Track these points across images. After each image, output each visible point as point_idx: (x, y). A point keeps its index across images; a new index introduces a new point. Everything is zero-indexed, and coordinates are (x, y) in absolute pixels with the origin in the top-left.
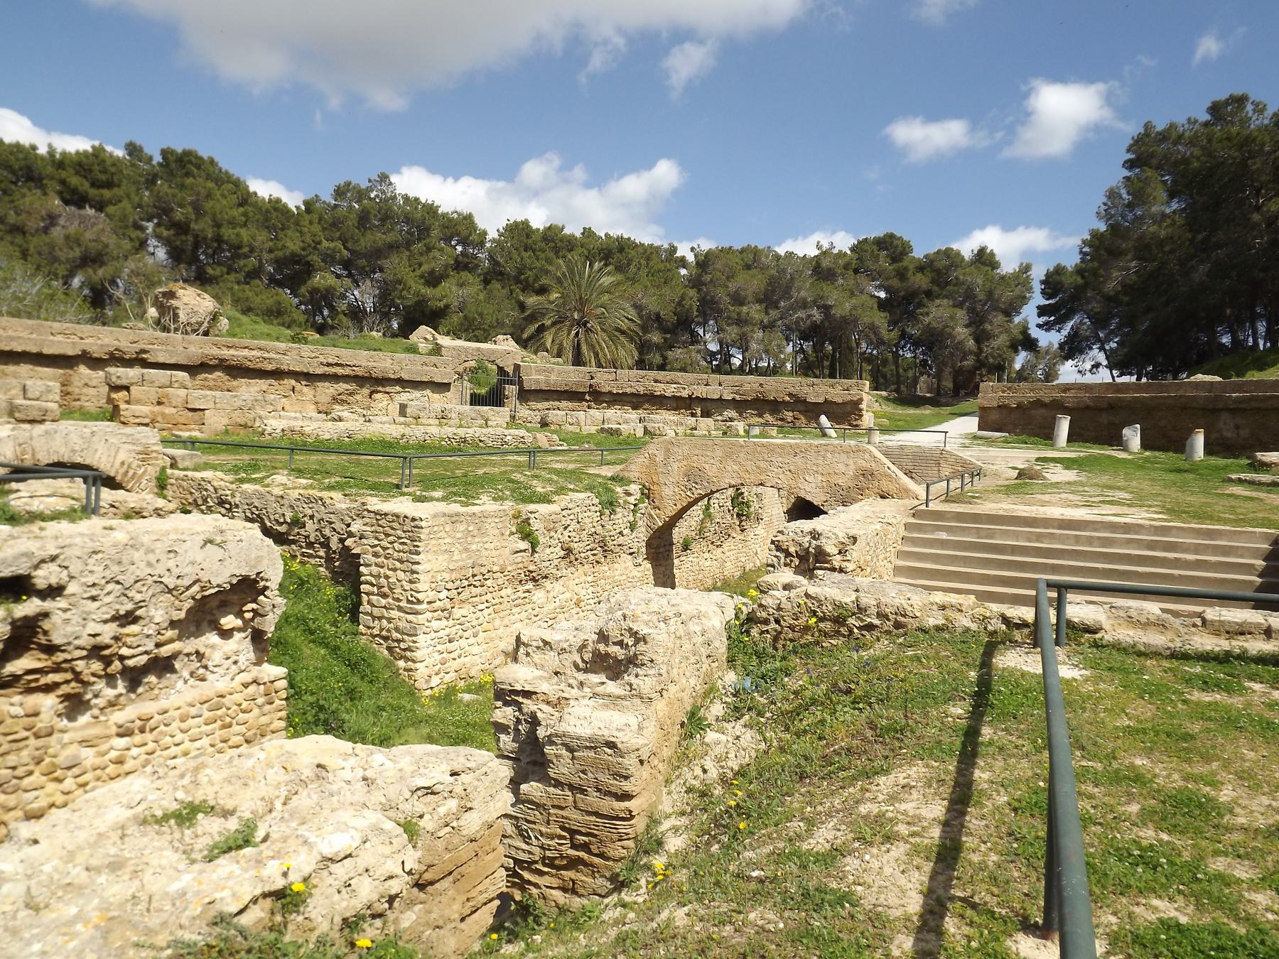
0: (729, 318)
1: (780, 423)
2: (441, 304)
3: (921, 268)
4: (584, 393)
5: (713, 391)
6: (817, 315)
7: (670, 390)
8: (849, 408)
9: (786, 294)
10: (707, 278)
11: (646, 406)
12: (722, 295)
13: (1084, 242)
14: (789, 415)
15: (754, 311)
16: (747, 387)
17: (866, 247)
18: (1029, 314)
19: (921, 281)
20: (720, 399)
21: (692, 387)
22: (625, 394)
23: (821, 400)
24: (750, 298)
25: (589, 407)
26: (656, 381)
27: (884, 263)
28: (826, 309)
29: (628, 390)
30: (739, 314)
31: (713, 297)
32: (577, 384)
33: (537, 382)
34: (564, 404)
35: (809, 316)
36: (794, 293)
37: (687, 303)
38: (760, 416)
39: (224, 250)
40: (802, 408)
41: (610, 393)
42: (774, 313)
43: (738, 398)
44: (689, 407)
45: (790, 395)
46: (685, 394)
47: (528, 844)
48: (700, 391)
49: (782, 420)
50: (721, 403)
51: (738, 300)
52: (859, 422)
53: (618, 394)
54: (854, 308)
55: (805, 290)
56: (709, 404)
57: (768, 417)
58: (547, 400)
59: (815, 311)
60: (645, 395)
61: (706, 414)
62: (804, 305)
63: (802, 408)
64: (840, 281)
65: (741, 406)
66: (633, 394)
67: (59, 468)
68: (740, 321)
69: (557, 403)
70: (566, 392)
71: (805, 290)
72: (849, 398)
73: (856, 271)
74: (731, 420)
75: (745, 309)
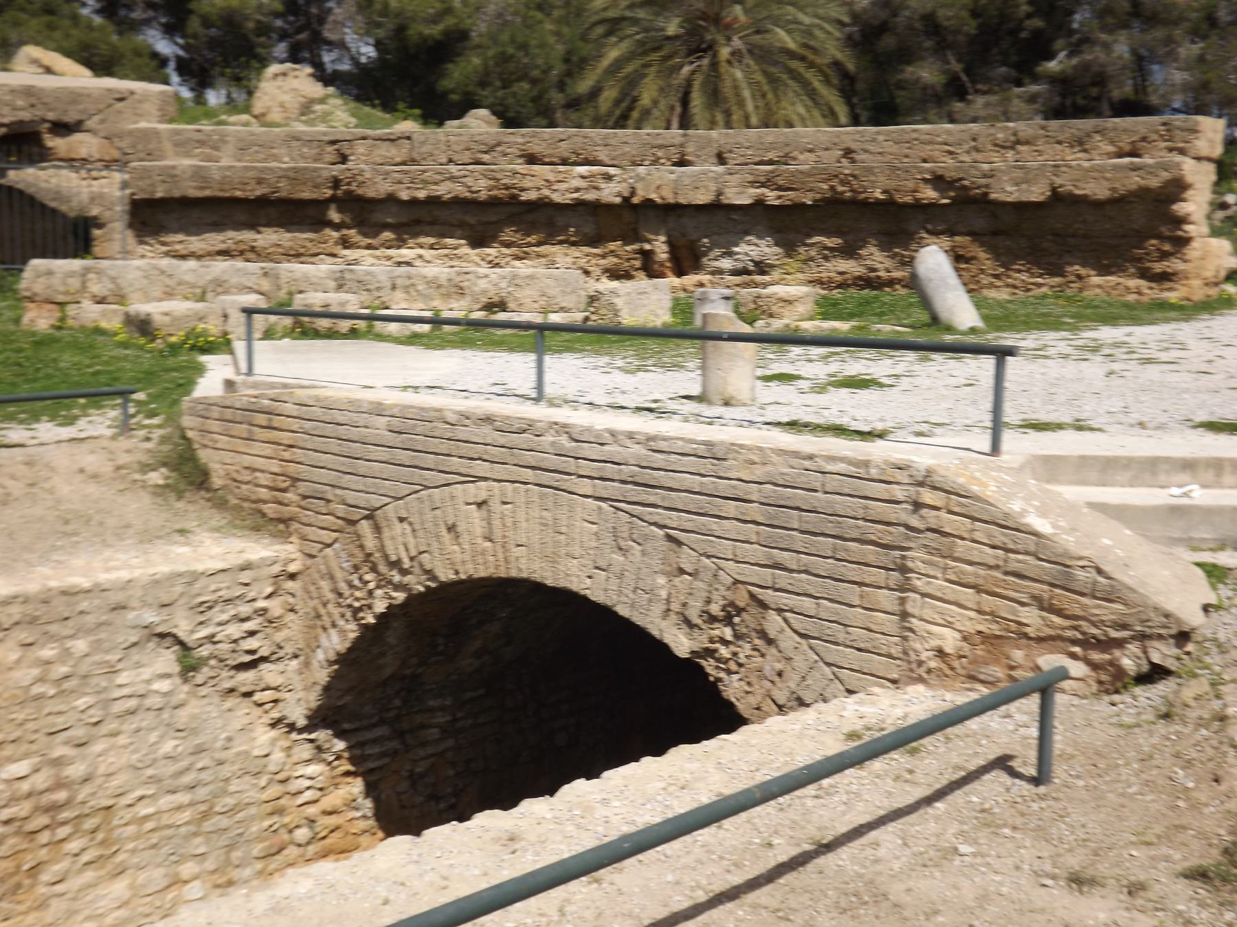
2: (435, 31)
4: (323, 204)
5: (698, 183)
7: (568, 184)
11: (508, 234)
16: (805, 162)
20: (716, 207)
22: (433, 201)
23: (1037, 193)
25: (346, 243)
26: (532, 159)
29: (445, 190)
32: (295, 176)
33: (170, 175)
34: (268, 237)
38: (849, 251)
39: (1185, 87)
40: (980, 223)
41: (391, 199)
43: (772, 197)
44: (632, 235)
45: (938, 181)
46: (610, 193)
47: (357, 809)
48: (660, 182)
52: (1175, 265)
53: (414, 202)
57: (876, 259)
58: (218, 227)
60: (493, 203)
61: (685, 259)
65: (788, 223)
66: (457, 202)
67: (324, 838)
69: (247, 235)
70: (262, 201)
72: (1135, 181)
74: (762, 267)
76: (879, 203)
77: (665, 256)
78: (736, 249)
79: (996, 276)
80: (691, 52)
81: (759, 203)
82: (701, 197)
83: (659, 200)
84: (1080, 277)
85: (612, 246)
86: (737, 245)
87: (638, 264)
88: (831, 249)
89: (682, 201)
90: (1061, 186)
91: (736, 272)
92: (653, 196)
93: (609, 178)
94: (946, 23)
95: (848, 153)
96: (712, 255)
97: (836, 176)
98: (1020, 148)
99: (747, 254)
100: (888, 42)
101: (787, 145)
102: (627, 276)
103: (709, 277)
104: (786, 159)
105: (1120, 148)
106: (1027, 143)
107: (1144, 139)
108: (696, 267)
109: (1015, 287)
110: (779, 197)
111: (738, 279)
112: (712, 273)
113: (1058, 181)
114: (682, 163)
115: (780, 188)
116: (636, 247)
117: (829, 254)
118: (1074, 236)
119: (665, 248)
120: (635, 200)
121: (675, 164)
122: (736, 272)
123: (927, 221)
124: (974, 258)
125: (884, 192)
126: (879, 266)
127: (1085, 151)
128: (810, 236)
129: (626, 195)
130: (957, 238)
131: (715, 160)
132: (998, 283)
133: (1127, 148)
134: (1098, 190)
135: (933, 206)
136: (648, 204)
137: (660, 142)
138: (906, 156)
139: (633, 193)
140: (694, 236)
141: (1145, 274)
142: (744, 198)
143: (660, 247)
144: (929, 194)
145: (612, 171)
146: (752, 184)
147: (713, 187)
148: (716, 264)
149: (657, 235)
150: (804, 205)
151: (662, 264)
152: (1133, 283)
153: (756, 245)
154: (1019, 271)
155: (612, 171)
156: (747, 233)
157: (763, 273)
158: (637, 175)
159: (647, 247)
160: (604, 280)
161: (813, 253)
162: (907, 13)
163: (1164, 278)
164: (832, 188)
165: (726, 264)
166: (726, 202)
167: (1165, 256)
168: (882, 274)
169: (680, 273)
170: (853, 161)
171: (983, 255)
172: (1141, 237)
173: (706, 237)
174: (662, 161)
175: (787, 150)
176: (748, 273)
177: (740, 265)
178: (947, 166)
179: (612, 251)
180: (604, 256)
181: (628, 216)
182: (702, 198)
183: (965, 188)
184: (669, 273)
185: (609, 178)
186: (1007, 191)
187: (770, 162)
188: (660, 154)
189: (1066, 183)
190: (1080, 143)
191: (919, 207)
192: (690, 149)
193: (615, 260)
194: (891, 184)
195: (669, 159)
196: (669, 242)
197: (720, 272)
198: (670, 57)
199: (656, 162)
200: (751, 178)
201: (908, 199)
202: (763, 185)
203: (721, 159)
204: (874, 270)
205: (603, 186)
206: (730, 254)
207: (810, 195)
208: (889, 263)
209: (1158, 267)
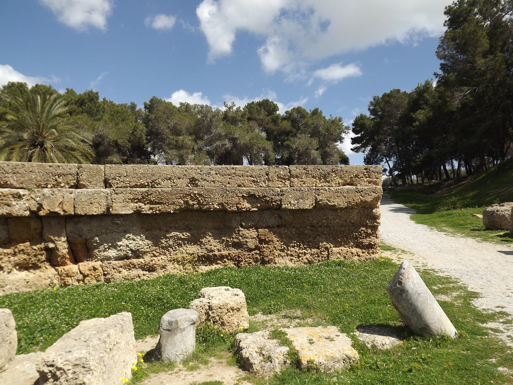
0: (170, 144)
1: (234, 252)
3: (284, 119)
5: (92, 199)
6: (228, 145)
8: (354, 216)
9: (208, 131)
10: (153, 116)
12: (163, 127)
13: (371, 103)
14: (250, 235)
15: (188, 140)
16: (166, 187)
17: (252, 106)
18: (346, 146)
19: (287, 125)
21: (38, 193)
23: (308, 204)
24: (184, 131)
27: (263, 115)
28: (233, 140)
30: (177, 141)
31: (157, 129)
35: (223, 145)
36: (214, 131)
37: (138, 133)
38: (195, 240)
40: (272, 221)
42: (200, 143)
43: (146, 209)
44: (38, 237)
45: (251, 197)
48: (60, 200)
49: (237, 245)
50: (111, 224)
51: (176, 132)
52: (373, 240)
54: (252, 139)
55: (220, 129)
56: (84, 228)
57: (213, 244)
59: (227, 142)
61: (80, 252)
62: (219, 137)
63: (272, 221)
64: (240, 124)
68: (179, 147)
71: (220, 129)
72: (358, 198)
73: (249, 119)
75: (181, 138)
76: (215, 210)
77: (65, 251)
78: (119, 243)
79: (282, 250)
80: (31, 146)
81: (138, 213)
82: (95, 210)
83: (62, 213)
84: (327, 249)
85: (21, 246)
86: (120, 240)
87: (43, 258)
88: (183, 240)
89: (79, 212)
90: (321, 200)
91: (119, 258)
92: (57, 210)
93: (19, 197)
94: (120, 144)
95: (193, 181)
96: (101, 248)
97: (190, 195)
98: (292, 179)
99: (127, 246)
100: (101, 148)
101: (153, 175)
102: (35, 267)
103: (100, 263)
104: (153, 184)
105: (346, 181)
106: (297, 177)
107: (356, 176)
108: (89, 255)
109: (292, 255)
110: (151, 209)
111: (121, 263)
112: (102, 260)
113: (319, 198)
114: (77, 186)
115: (151, 203)
116: (43, 245)
117: (180, 242)
118: (321, 226)
119: (66, 245)
120: (42, 213)
121: (71, 187)
122: (119, 258)
123: (242, 221)
124: (270, 241)
125: (219, 205)
126: (213, 248)
127: (329, 182)
128: (168, 232)
129: (35, 209)
130: (260, 230)
131: (103, 185)
132: (283, 254)
133: (349, 181)
134: (340, 202)
135: (248, 211)
136: (53, 215)
137: (60, 171)
138: (229, 183)
139: (40, 207)
140: (88, 237)
141: (358, 245)
142: (128, 210)
143: (62, 245)
144: (246, 205)
145: (21, 192)
146: (133, 200)
147: (104, 203)
148: (102, 253)
149: (59, 237)
150: (170, 212)
151: (64, 257)
152: (354, 250)
153: (134, 240)
154: (294, 247)
155: (21, 192)
156: (126, 232)
157: (138, 257)
158: (44, 195)
159: (51, 245)
160: (15, 271)
161: (171, 243)
162: (108, 140)
163: (370, 246)
164: (186, 202)
165: (112, 253)
166: (113, 212)
167: (368, 235)
168: (217, 253)
169: (76, 261)
170: (197, 186)
171: (275, 239)
172: (356, 226)
173: (97, 236)
174: (62, 185)
175: (154, 178)
176: (127, 257)
177: (122, 254)
178: (253, 189)
179: (23, 250)
180: (15, 254)
181: (34, 224)
182: (96, 210)
183: (267, 202)
184: (68, 262)
185: (19, 197)
186: (291, 202)
187: (142, 186)
188: (60, 180)
189: (323, 198)
190: (325, 177)
191: (240, 212)
192: (84, 177)
193: (25, 257)
194: (221, 200)
195: (68, 184)
196: (68, 241)
197: (109, 259)
198: (25, 146)
199: (57, 185)
200: (131, 197)
201: (234, 208)
202: (139, 201)
203: (107, 184)
204: (212, 251)
205: (14, 203)
206: (115, 247)
207: (172, 207)
208: (219, 246)
209: (366, 241)
